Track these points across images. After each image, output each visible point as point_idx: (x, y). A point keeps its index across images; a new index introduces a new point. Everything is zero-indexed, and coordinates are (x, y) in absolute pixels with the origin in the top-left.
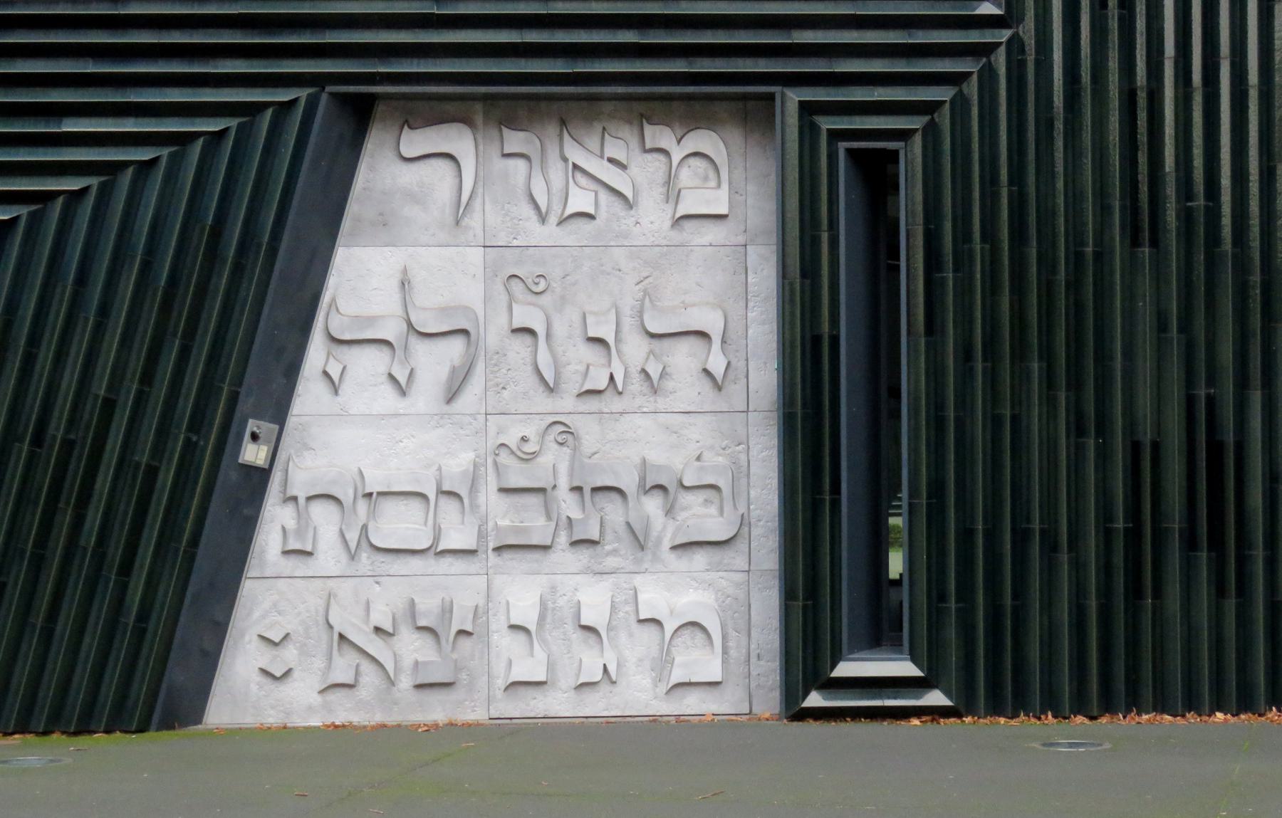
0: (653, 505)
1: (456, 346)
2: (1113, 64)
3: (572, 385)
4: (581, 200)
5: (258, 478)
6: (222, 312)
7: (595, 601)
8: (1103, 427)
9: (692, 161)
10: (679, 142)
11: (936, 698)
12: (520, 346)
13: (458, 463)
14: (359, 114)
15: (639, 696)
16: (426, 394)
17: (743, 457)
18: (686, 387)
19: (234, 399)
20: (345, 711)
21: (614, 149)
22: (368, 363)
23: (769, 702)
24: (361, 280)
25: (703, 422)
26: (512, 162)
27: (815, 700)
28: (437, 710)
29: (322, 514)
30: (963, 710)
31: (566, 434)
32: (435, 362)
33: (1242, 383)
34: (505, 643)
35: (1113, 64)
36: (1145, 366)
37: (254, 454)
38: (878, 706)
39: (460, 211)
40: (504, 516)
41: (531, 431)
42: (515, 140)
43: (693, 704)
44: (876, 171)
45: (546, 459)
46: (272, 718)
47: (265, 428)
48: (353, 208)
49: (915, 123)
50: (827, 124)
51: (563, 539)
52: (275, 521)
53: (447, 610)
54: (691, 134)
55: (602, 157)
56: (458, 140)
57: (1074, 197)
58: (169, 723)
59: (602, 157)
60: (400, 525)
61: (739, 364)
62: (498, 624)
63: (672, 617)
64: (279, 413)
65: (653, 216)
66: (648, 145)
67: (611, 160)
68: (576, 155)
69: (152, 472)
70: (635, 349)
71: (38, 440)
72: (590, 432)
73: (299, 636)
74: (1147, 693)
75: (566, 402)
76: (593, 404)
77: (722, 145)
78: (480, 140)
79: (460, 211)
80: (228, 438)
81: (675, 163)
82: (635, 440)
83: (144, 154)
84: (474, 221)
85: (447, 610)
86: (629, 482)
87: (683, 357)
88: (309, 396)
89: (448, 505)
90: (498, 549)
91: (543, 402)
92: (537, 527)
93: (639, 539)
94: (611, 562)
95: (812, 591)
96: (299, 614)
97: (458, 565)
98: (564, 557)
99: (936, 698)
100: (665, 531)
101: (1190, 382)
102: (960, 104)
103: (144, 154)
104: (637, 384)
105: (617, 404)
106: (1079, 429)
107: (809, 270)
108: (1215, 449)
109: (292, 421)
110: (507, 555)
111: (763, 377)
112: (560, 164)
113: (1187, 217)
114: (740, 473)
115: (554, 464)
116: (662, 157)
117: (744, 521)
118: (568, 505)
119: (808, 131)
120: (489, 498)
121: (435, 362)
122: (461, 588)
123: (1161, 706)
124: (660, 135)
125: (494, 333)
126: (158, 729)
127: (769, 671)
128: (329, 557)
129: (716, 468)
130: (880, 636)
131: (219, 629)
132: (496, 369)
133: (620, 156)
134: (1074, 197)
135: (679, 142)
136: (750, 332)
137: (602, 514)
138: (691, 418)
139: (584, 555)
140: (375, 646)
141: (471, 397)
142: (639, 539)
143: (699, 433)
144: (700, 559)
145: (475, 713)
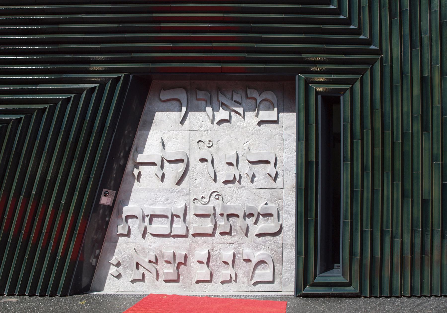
3: (221, 178)
9: (264, 102)
10: (260, 95)
11: (352, 289)
13: (179, 207)
16: (170, 179)
17: (281, 204)
26: (200, 102)
27: (308, 290)
32: (173, 171)
54: (263, 93)
55: (232, 100)
59: (232, 100)
61: (280, 173)
66: (249, 96)
67: (235, 101)
70: (245, 168)
74: (426, 292)
77: (275, 96)
78: (189, 94)
81: (258, 103)
83: (40, 107)
90: (194, 235)
94: (236, 239)
96: (123, 255)
100: (256, 230)
103: (40, 107)
107: (308, 163)
109: (121, 189)
110: (198, 238)
112: (217, 103)
116: (254, 101)
126: (71, 294)
132: (193, 172)
133: (239, 100)
135: (260, 95)
136: (284, 161)
138: (262, 190)
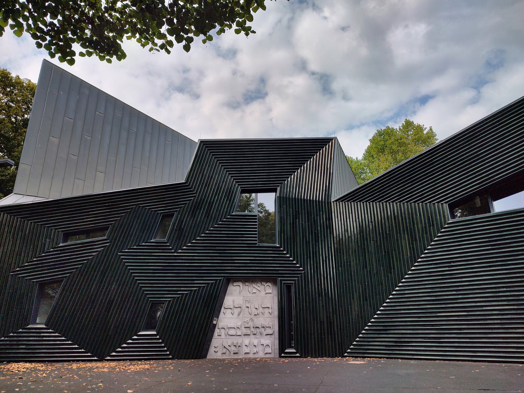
0: (263, 329)
1: (239, 309)
2: (316, 275)
4: (254, 291)
5: (215, 326)
6: (213, 304)
7: (256, 342)
8: (317, 320)
11: (298, 355)
12: (247, 309)
13: (239, 324)
14: (230, 280)
15: (261, 355)
16: (236, 315)
18: (267, 314)
19: (213, 315)
20: (224, 357)
21: (258, 285)
22: (229, 311)
23: (277, 355)
24: (229, 300)
25: (270, 320)
27: (283, 355)
28: (236, 357)
29: (222, 330)
30: (223, 177)
31: (252, 320)
33: (333, 314)
34: (244, 347)
35: (316, 275)
36: (321, 313)
37: (215, 322)
38: (290, 356)
39: (240, 292)
40: (245, 331)
41: (248, 319)
42: (247, 284)
43: (268, 356)
44: (289, 287)
45: (250, 324)
46: (215, 358)
47: (216, 319)
48: (227, 292)
49: (293, 282)
50: (283, 282)
51: (252, 334)
52: (217, 331)
53: (237, 343)
56: (240, 284)
57: (312, 291)
58: (202, 358)
60: (232, 332)
62: (244, 345)
63: (264, 344)
64: (218, 318)
65: (263, 293)
68: (254, 285)
69: (203, 324)
70: (261, 310)
71: (189, 321)
72: (255, 320)
73: (220, 346)
75: (252, 316)
76: (255, 316)
79: (240, 292)
80: (212, 321)
82: (260, 321)
84: (242, 293)
85: (237, 343)
86: (260, 326)
87: (266, 311)
88: (221, 315)
89: (238, 329)
91: (250, 316)
92: (248, 332)
93: (261, 334)
94: (258, 337)
95: (282, 341)
97: (239, 337)
98: (252, 336)
99: (298, 355)
101: (327, 314)
102: (298, 280)
104: (261, 314)
105: (258, 316)
106: (314, 320)
108: (330, 322)
111: (276, 313)
113: (325, 293)
114: (273, 325)
115: (251, 324)
117: (274, 332)
118: (252, 329)
119: (281, 283)
120: (243, 328)
121: (237, 311)
122: (239, 340)
123: (326, 356)
124: (264, 283)
125: (244, 307)
127: (277, 351)
128: (223, 336)
129: (270, 325)
130: (291, 347)
131: (209, 345)
134: (312, 291)
137: (255, 330)
139: (254, 336)
140: (228, 348)
141: (241, 316)
142: (261, 334)
143: (268, 320)
144: (269, 336)
145: (241, 357)
